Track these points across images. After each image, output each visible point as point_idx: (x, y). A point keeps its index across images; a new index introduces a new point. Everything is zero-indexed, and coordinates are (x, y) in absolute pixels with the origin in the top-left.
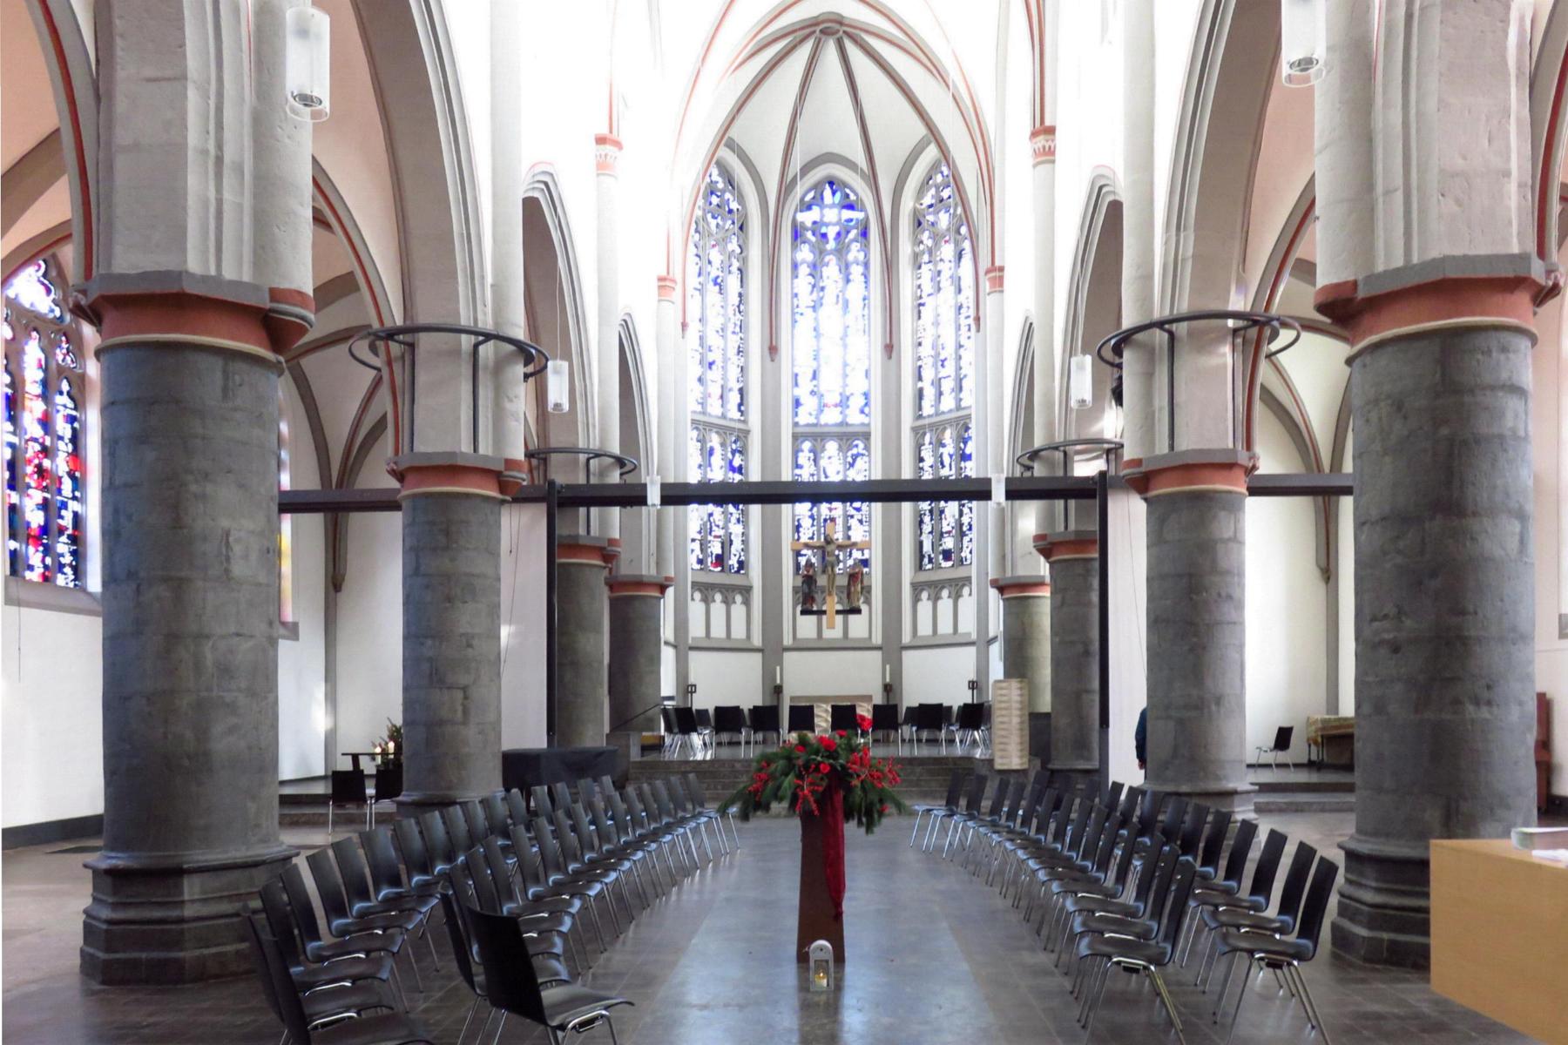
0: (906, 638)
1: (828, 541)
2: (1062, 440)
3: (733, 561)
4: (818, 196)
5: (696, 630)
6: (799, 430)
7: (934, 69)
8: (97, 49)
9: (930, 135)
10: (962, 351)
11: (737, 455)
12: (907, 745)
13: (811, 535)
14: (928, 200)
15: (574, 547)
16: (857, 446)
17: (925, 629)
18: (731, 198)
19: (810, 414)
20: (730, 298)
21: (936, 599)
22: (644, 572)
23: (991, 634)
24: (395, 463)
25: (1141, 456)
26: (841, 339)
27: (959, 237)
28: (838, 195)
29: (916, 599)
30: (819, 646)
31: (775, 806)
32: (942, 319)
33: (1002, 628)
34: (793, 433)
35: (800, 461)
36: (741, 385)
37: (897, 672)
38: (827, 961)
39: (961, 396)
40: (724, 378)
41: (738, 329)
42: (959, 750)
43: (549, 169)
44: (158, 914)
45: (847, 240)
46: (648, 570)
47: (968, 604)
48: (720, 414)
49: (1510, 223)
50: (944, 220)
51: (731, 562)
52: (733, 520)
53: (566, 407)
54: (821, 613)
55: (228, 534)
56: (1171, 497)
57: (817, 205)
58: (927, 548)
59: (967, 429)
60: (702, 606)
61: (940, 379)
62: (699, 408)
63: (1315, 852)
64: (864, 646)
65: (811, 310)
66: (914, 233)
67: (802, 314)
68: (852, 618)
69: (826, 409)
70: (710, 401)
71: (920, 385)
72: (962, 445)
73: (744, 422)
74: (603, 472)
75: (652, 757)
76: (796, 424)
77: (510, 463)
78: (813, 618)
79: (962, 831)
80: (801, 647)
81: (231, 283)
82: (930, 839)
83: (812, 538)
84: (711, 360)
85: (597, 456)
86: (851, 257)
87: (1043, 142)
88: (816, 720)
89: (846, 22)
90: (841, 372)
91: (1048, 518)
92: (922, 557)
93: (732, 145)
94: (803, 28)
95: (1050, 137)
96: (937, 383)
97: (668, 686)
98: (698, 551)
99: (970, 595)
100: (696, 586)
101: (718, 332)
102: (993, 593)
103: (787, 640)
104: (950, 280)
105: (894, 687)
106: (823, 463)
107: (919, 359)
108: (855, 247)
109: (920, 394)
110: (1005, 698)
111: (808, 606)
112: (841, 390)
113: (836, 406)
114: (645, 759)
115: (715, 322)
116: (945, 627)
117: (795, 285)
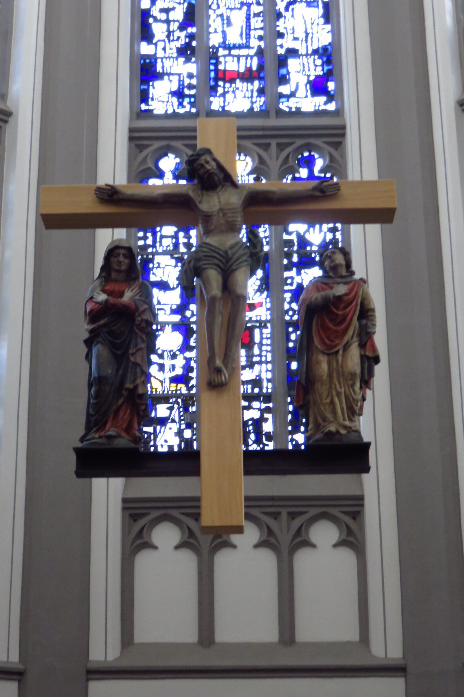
13: (179, 371)
34: (131, 130)
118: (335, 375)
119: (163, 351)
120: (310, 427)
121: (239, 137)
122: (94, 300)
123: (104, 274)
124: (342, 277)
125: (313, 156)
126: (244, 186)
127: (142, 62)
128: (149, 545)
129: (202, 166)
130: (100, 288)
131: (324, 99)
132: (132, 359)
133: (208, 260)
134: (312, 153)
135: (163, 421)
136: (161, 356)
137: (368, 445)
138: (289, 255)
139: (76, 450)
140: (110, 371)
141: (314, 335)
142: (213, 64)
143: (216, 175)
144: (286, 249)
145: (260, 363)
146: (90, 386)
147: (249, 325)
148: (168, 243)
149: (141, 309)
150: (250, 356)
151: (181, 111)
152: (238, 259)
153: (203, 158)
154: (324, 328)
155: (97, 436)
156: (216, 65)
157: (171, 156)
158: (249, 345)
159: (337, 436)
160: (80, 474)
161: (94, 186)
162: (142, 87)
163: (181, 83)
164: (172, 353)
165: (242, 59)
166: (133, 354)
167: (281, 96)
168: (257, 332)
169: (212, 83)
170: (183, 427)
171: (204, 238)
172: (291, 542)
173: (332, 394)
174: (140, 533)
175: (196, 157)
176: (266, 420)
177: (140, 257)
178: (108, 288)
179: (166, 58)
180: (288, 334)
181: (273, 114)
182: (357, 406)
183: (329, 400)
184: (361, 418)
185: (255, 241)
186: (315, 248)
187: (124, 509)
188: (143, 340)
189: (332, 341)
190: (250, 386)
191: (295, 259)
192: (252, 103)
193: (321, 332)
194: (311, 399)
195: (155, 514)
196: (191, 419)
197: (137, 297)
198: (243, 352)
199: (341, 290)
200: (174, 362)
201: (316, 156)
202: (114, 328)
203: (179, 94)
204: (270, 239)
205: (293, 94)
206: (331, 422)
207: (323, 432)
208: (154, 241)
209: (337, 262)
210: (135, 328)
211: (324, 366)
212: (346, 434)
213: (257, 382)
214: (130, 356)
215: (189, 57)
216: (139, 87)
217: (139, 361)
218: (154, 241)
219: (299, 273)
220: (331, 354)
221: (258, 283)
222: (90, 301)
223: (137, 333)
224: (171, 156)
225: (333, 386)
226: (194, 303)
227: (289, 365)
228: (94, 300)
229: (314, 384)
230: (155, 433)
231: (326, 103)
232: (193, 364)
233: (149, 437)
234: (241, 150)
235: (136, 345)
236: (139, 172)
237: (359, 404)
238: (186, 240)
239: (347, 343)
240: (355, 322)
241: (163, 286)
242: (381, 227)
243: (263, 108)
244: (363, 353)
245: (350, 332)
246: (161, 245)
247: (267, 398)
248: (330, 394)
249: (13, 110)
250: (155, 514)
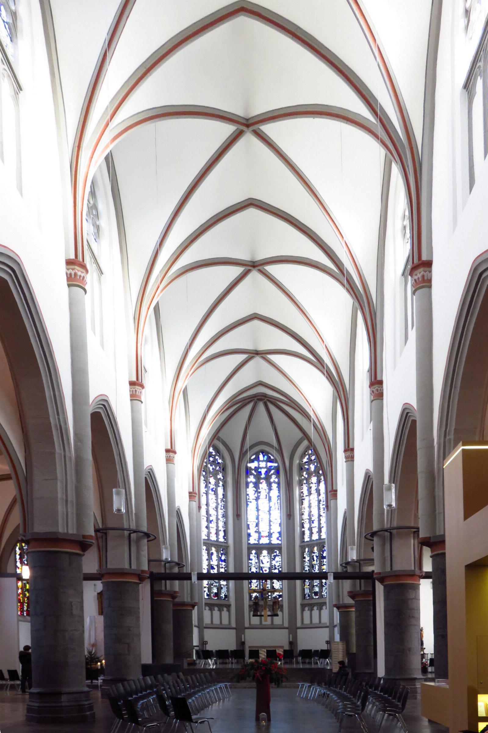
0: (299, 624)
1: (264, 589)
2: (389, 526)
3: (223, 595)
4: (257, 458)
5: (207, 620)
6: (250, 546)
7: (375, 40)
8: (26, 469)
9: (305, 437)
10: (321, 518)
11: (223, 556)
12: (299, 664)
13: (256, 586)
14: (305, 460)
15: (161, 593)
16: (276, 552)
17: (307, 621)
18: (219, 458)
19: (255, 540)
20: (219, 496)
21: (311, 610)
22: (186, 600)
23: (335, 623)
24: (100, 571)
25: (380, 571)
26: (268, 511)
27: (319, 475)
28: (266, 457)
29: (303, 610)
30: (261, 627)
31: (248, 678)
32: (313, 505)
33: (338, 622)
34: (248, 547)
35: (251, 557)
36: (225, 529)
37: (295, 637)
38: (265, 718)
39: (321, 534)
40: (217, 526)
41: (222, 508)
42: (319, 666)
43: (106, 398)
44: (54, 705)
45: (270, 474)
46: (187, 599)
47: (325, 612)
48: (215, 540)
50: (312, 467)
51: (221, 596)
53: (123, 510)
54: (261, 616)
55: (71, 603)
56: (392, 585)
57: (257, 461)
58: (307, 591)
59: (324, 547)
60: (209, 612)
61: (312, 528)
62: (206, 538)
64: (282, 627)
65: (255, 500)
66: (299, 472)
67: (251, 502)
68: (275, 618)
69: (262, 538)
70: (211, 535)
71: (303, 529)
72: (322, 553)
73: (226, 543)
74: (171, 568)
75: (191, 667)
77: (143, 571)
78: (258, 618)
79: (317, 690)
80: (252, 627)
81: (71, 534)
82: (304, 695)
83: (257, 587)
84: (211, 520)
85: (135, 532)
86: (272, 480)
87: (422, 273)
88: (260, 655)
89: (267, 396)
90: (268, 524)
91: (354, 585)
92: (305, 595)
93: (219, 439)
94: (248, 399)
95: (380, 386)
96: (310, 529)
97: (196, 642)
98: (207, 592)
99: (326, 609)
100: (206, 604)
101: (214, 509)
102: (335, 609)
103: (247, 625)
104: (315, 491)
106: (261, 558)
107: (303, 520)
108: (274, 477)
109: (303, 533)
110: (337, 648)
111: (256, 613)
112: (269, 531)
113: (266, 537)
114: (189, 668)
115: (212, 505)
116: (316, 620)
117: (247, 491)
138: (273, 568)
148: (254, 565)
165: (254, 490)
191: (274, 568)
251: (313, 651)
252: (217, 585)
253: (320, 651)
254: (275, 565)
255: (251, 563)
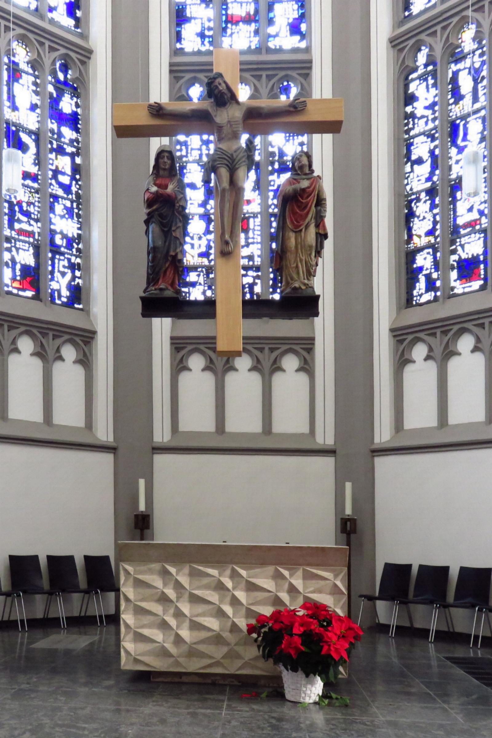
13: (203, 249)
34: (171, 65)
49: (106, 631)
51: (54, 285)
52: (59, 208)
63: (36, 557)
76: (177, 52)
105: (359, 523)
118: (299, 246)
119: (194, 234)
120: (283, 284)
121: (241, 70)
122: (149, 191)
123: (155, 172)
124: (306, 174)
125: (290, 85)
126: (243, 104)
127: (177, 8)
128: (186, 368)
129: (217, 87)
130: (153, 183)
131: (298, 38)
132: (174, 234)
133: (222, 161)
134: (290, 83)
135: (193, 284)
136: (192, 238)
137: (318, 297)
138: (272, 163)
139: (142, 299)
140: (160, 243)
141: (287, 217)
142: (224, 9)
143: (226, 94)
144: (271, 159)
145: (253, 243)
146: (149, 253)
147: (247, 215)
149: (179, 197)
150: (247, 238)
151: (203, 49)
152: (239, 160)
153: (217, 80)
154: (294, 213)
155: (153, 288)
156: (226, 10)
157: (197, 85)
158: (246, 230)
159: (300, 291)
160: (144, 315)
161: (147, 103)
162: (178, 29)
163: (203, 25)
164: (199, 236)
166: (174, 231)
167: (270, 36)
168: (251, 220)
169: (224, 25)
170: (206, 288)
171: (218, 144)
172: (271, 367)
173: (297, 261)
174: (181, 361)
175: (213, 80)
176: (256, 284)
177: (178, 165)
178: (157, 182)
179: (193, 4)
180: (271, 222)
181: (264, 51)
182: (312, 269)
183: (295, 265)
184: (315, 278)
185: (251, 147)
186: (289, 158)
187: (172, 344)
188: (180, 221)
189: (298, 222)
190: (247, 260)
191: (276, 166)
192: (251, 42)
193: (292, 216)
194: (284, 264)
195: (190, 347)
196: (211, 283)
197: (176, 189)
198: (242, 236)
199: (305, 184)
200: (200, 242)
201: (292, 85)
202: (163, 211)
203: (202, 35)
204: (261, 151)
205: (277, 35)
206: (296, 280)
207: (291, 288)
208: (187, 153)
209: (303, 163)
210: (175, 212)
211: (293, 240)
212: (305, 289)
213: (251, 258)
214: (173, 232)
215: (208, 3)
216: (175, 29)
217: (178, 236)
218: (187, 153)
219: (279, 177)
220: (297, 231)
221: (253, 184)
222: (147, 192)
223: (176, 216)
224: (197, 85)
225: (298, 255)
226: (213, 199)
227: (271, 245)
228: (149, 191)
229: (286, 253)
230: (189, 293)
231: (300, 41)
232: (212, 244)
233: (186, 295)
234: (243, 81)
235: (176, 224)
236: (177, 98)
237: (314, 268)
238: (207, 152)
239: (307, 224)
240: (313, 208)
241: (193, 186)
242: (333, 136)
243: (258, 46)
244: (317, 231)
245: (310, 216)
246: (191, 156)
247: (258, 269)
248: (296, 261)
249: (93, 49)
250: (190, 347)
251: (415, 570)
252: (36, 230)
253: (415, 570)
254: (282, 154)
255: (185, 144)
